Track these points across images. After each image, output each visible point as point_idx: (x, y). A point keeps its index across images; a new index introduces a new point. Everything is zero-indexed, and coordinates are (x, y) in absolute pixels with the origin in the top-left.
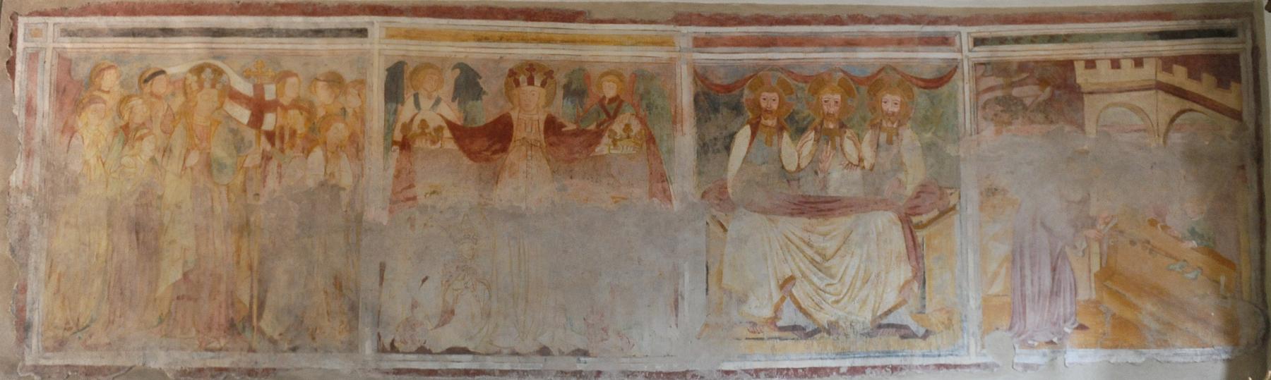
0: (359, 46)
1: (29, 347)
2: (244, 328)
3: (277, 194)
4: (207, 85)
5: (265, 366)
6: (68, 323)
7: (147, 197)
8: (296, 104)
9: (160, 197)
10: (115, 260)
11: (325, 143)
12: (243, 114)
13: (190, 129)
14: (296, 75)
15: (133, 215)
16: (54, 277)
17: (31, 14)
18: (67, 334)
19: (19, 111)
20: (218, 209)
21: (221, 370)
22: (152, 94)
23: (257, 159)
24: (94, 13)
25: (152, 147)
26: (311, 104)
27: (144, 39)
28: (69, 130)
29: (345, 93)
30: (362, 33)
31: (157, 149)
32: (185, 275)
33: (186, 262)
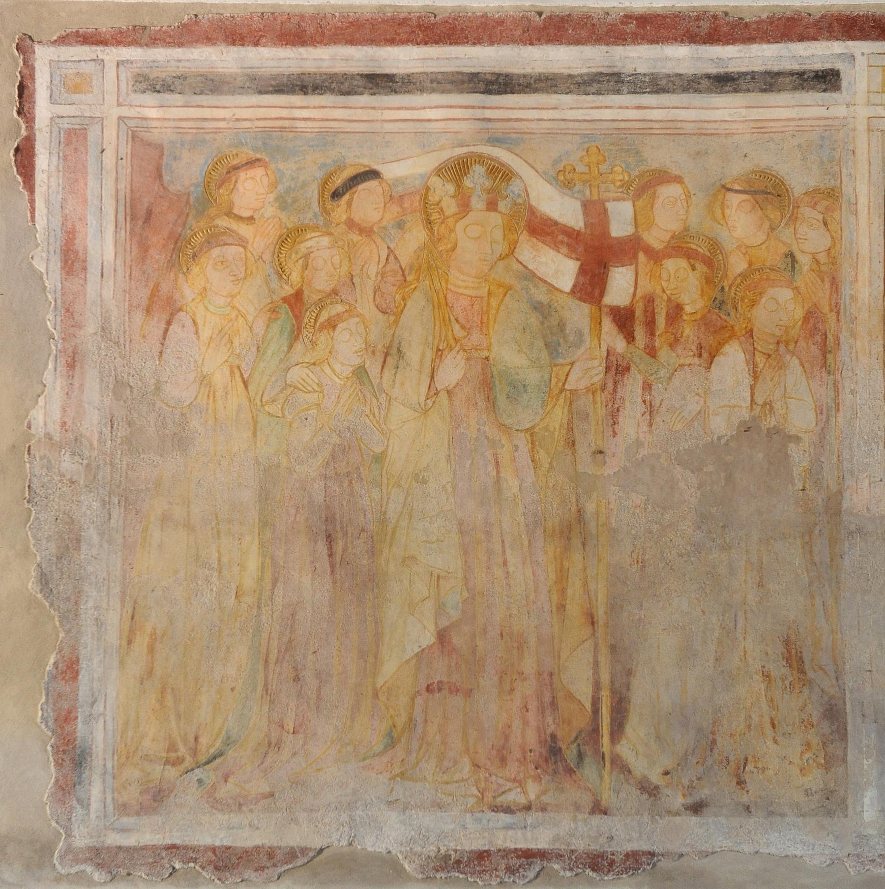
0: (822, 112)
1: (85, 804)
2: (581, 756)
3: (644, 452)
4: (478, 203)
5: (630, 847)
6: (172, 748)
7: (351, 461)
8: (679, 246)
9: (379, 459)
10: (279, 600)
11: (750, 333)
12: (561, 270)
13: (441, 305)
14: (678, 180)
15: (319, 497)
16: (141, 642)
17: (63, 40)
18: (172, 772)
19: (46, 263)
20: (511, 484)
21: (528, 855)
22: (351, 224)
23: (597, 374)
24: (209, 40)
25: (359, 344)
26: (715, 245)
27: (327, 99)
28: (164, 307)
29: (794, 219)
30: (827, 80)
31: (369, 349)
32: (442, 637)
33: (440, 608)
